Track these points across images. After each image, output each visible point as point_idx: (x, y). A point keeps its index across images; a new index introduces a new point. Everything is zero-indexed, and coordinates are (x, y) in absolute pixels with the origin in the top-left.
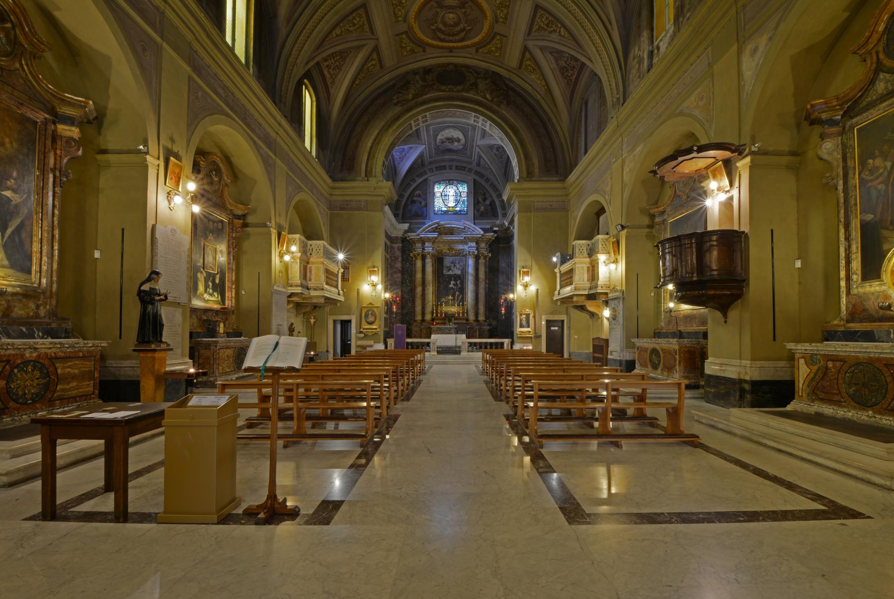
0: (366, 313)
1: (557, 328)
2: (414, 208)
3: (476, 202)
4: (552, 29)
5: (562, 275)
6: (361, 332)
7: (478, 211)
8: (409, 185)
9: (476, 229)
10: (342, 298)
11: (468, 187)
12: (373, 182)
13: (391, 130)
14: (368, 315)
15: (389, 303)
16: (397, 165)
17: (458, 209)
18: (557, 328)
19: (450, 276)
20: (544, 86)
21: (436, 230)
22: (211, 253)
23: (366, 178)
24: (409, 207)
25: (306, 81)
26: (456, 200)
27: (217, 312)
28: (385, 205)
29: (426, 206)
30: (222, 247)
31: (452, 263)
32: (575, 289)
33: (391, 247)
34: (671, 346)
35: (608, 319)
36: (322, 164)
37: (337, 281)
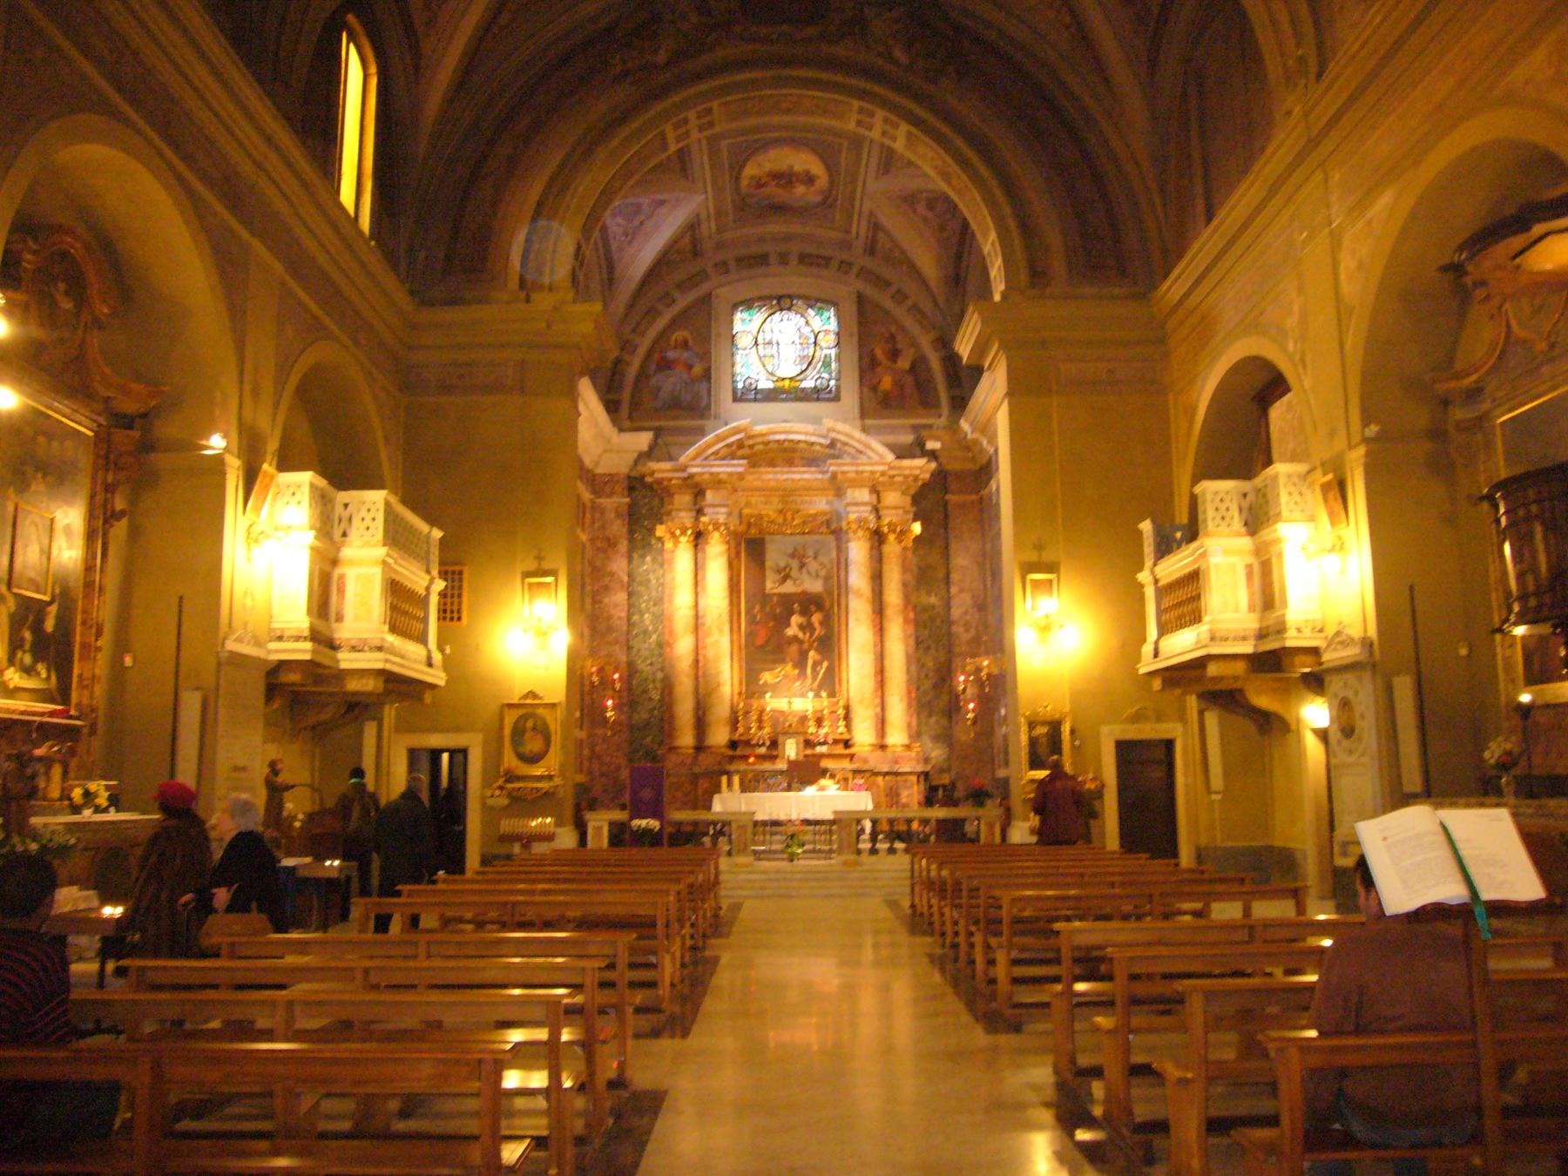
2: (669, 383)
3: (867, 360)
5: (1162, 591)
7: (874, 389)
8: (652, 313)
9: (868, 446)
10: (438, 677)
11: (839, 316)
12: (543, 301)
13: (602, 153)
14: (524, 731)
15: (587, 682)
16: (615, 257)
20: (1067, 27)
21: (740, 453)
22: (34, 537)
23: (522, 295)
24: (654, 381)
25: (351, 18)
27: (45, 731)
28: (582, 374)
29: (707, 375)
30: (71, 517)
31: (793, 556)
32: (1212, 639)
33: (595, 507)
34: (1551, 822)
35: (1323, 735)
36: (392, 259)
37: (425, 620)
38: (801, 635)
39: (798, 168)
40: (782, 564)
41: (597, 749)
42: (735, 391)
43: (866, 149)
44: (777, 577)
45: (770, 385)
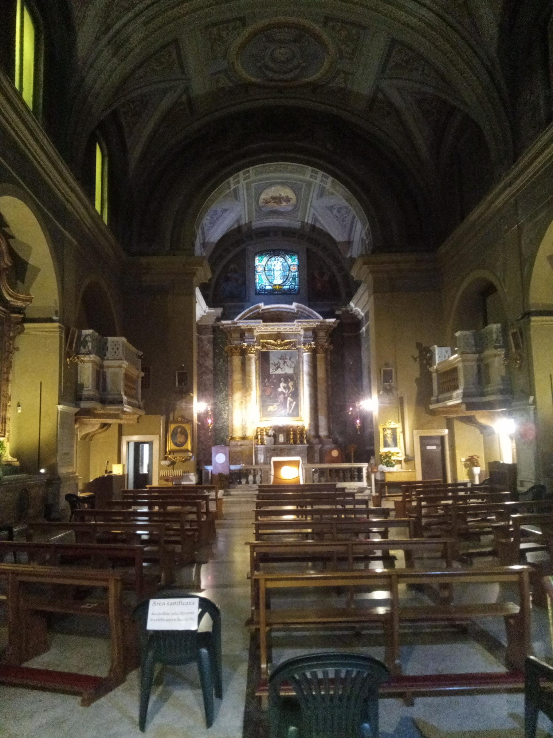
0: (173, 431)
1: (434, 447)
4: (412, 67)
6: (166, 459)
9: (312, 313)
17: (287, 287)
18: (434, 447)
19: (279, 377)
26: (284, 276)
31: (281, 359)
38: (284, 391)
39: (283, 195)
40: (276, 362)
41: (201, 439)
42: (256, 290)
43: (313, 188)
44: (274, 367)
45: (270, 288)
